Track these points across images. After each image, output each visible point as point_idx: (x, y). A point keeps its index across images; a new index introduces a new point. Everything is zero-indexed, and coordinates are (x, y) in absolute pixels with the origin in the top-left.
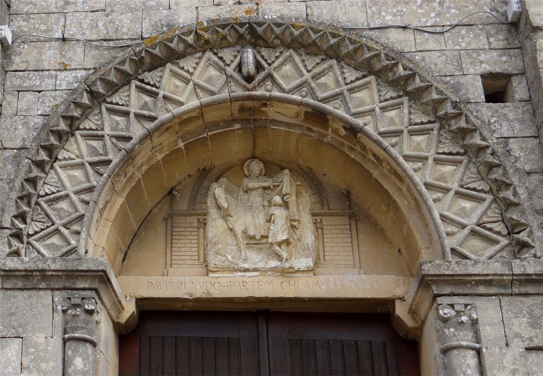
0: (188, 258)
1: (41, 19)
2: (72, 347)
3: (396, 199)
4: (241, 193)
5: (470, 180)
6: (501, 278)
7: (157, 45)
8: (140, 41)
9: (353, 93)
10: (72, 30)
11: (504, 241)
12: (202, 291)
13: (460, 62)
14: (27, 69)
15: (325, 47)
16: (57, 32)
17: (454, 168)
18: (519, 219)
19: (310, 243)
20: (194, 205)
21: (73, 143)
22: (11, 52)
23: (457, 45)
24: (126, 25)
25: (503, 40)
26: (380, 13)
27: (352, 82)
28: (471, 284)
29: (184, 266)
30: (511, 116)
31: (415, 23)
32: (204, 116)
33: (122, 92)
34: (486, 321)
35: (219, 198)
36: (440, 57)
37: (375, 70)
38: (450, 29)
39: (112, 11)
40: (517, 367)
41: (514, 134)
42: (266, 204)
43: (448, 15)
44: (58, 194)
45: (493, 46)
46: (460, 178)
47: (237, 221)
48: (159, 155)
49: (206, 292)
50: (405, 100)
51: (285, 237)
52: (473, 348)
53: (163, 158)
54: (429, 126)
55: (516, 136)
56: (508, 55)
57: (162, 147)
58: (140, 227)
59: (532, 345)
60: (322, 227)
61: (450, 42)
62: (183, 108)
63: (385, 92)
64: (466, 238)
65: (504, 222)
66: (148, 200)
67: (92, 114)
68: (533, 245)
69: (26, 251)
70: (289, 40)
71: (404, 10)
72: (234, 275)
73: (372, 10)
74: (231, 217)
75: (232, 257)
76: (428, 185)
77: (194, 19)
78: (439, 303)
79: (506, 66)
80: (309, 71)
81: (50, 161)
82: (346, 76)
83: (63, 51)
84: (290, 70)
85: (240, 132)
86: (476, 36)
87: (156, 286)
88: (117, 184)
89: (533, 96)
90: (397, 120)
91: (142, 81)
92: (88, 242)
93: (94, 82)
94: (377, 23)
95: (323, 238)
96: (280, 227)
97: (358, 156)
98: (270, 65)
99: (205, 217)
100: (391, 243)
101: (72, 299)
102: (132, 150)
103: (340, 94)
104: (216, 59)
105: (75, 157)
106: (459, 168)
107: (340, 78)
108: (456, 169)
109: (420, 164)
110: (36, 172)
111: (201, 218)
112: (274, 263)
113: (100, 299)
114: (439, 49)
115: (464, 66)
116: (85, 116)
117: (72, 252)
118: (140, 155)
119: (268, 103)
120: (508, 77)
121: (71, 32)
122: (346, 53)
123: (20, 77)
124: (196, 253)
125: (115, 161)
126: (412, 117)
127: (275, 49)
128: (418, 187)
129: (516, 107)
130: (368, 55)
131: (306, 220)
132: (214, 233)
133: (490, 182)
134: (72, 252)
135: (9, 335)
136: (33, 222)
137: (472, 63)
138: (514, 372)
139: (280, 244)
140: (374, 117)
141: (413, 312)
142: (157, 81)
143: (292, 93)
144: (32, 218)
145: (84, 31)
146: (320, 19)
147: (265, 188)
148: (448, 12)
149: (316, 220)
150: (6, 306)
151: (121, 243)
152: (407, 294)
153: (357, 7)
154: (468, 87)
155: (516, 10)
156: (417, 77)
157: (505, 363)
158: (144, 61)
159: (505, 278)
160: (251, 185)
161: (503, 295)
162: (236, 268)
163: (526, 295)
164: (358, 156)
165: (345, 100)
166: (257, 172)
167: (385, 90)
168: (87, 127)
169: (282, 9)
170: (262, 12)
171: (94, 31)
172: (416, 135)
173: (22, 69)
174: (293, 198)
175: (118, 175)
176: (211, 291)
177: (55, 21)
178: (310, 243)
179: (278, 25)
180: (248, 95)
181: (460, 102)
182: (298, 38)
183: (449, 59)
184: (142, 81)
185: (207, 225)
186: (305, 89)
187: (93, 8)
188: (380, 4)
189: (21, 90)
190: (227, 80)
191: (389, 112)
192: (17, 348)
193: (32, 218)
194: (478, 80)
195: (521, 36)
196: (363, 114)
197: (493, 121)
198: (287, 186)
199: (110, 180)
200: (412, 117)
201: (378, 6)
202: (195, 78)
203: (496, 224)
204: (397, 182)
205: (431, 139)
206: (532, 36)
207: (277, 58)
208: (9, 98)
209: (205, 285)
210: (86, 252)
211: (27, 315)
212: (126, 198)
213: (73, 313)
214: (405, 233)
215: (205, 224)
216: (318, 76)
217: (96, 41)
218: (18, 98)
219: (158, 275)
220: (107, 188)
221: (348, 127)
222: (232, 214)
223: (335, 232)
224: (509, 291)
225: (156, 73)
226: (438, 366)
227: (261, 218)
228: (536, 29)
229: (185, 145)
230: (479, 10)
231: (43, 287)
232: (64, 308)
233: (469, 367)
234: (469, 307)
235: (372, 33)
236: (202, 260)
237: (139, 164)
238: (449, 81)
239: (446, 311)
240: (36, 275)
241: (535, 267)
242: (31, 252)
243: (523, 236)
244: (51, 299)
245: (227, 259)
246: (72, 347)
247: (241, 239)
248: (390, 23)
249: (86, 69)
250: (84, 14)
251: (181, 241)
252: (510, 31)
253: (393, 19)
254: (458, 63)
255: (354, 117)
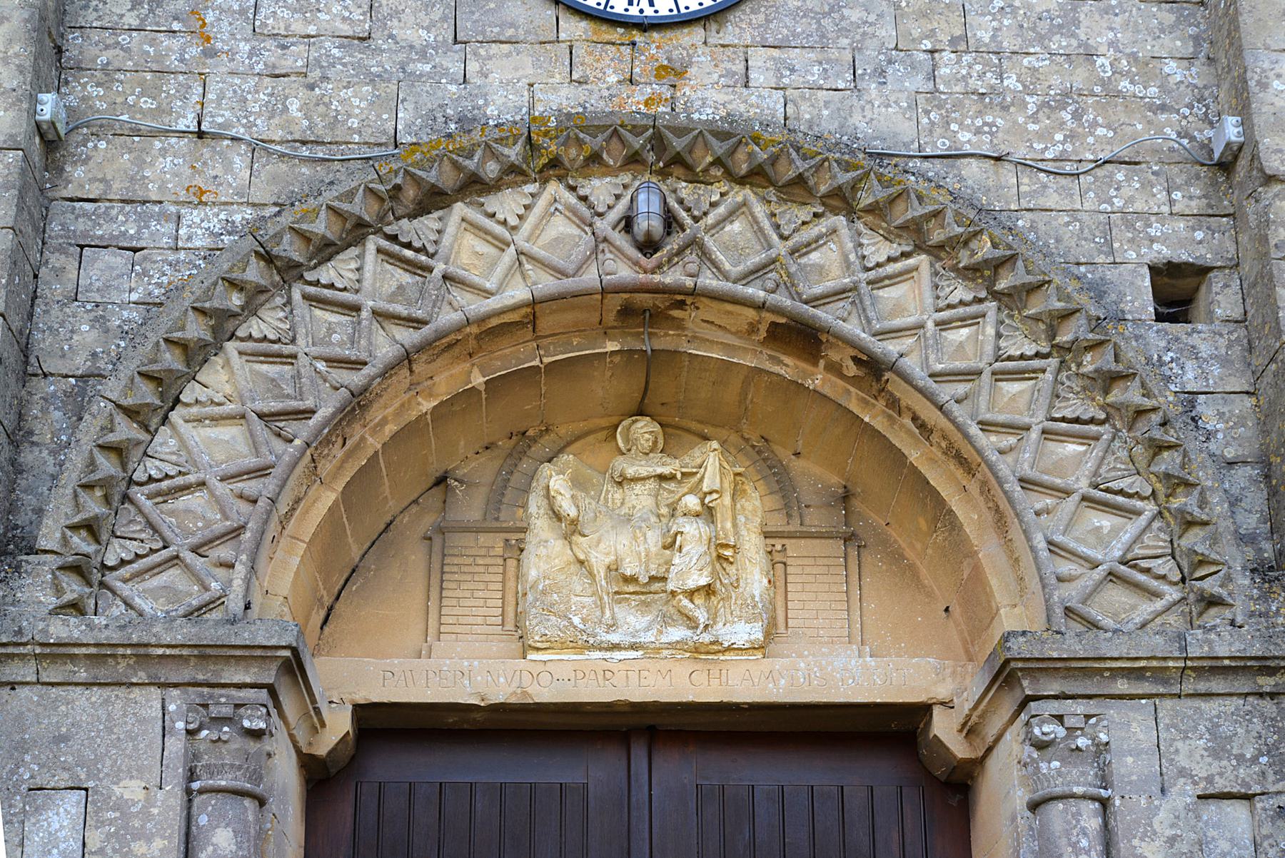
0: (480, 620)
1: (142, 83)
2: (210, 808)
3: (954, 509)
4: (608, 486)
5: (1113, 474)
6: (1163, 664)
7: (435, 161)
8: (391, 150)
9: (879, 288)
10: (223, 115)
11: (1172, 594)
12: (510, 690)
13: (1108, 237)
14: (104, 197)
15: (823, 189)
16: (185, 117)
17: (1082, 448)
18: (1207, 553)
19: (757, 593)
20: (499, 510)
21: (219, 368)
22: (64, 156)
23: (1104, 203)
24: (357, 111)
25: (1200, 198)
26: (948, 123)
27: (878, 265)
28: (1102, 676)
29: (470, 637)
30: (1205, 349)
31: (1020, 152)
32: (537, 322)
33: (343, 261)
34: (1125, 747)
35: (559, 498)
36: (1068, 224)
37: (930, 243)
38: (1092, 169)
39: (325, 78)
40: (1179, 832)
41: (1207, 386)
42: (664, 511)
43: (1091, 140)
44: (180, 481)
45: (1176, 209)
46: (1093, 469)
47: (597, 546)
48: (424, 402)
49: (519, 691)
50: (990, 308)
51: (703, 581)
52: (1093, 798)
53: (435, 407)
54: (1037, 363)
55: (1212, 390)
56: (1208, 228)
57: (434, 384)
58: (366, 553)
59: (1211, 791)
60: (784, 560)
61: (1092, 194)
62: (493, 303)
63: (948, 290)
64: (1097, 587)
65: (1174, 558)
66: (389, 497)
67: (268, 305)
68: (1232, 602)
69: (96, 604)
70: (744, 168)
71: (999, 121)
72: (586, 657)
73: (929, 119)
74: (584, 536)
75: (582, 619)
76: (1025, 482)
77: (524, 110)
78: (1034, 713)
79: (1202, 250)
80: (783, 238)
81: (161, 407)
82: (866, 253)
83: (197, 161)
84: (740, 233)
85: (617, 359)
86: (1146, 185)
87: (403, 678)
88: (323, 461)
89: (1251, 312)
90: (969, 349)
91: (393, 238)
92: (252, 586)
93: (278, 236)
94: (942, 146)
95: (786, 583)
96: (694, 561)
97: (879, 418)
98: (696, 219)
99: (521, 536)
100: (930, 595)
101: (211, 708)
102: (365, 389)
103: (850, 290)
104: (572, 200)
105: (223, 400)
106: (1093, 449)
107: (852, 257)
108: (1086, 452)
109: (1012, 440)
110: (126, 430)
111: (513, 537)
112: (677, 633)
113: (278, 705)
114: (1068, 208)
115: (1116, 245)
116: (250, 309)
117: (212, 606)
118: (382, 401)
119: (689, 300)
120: (1202, 271)
121: (220, 120)
122: (870, 205)
123: (85, 214)
124: (499, 595)
125: (324, 413)
126: (1002, 343)
127: (709, 187)
128: (1007, 486)
129: (1215, 333)
130: (919, 211)
131: (752, 544)
132: (541, 570)
133: (1154, 479)
134: (212, 606)
135: (52, 784)
136: (115, 540)
137: (1131, 241)
138: (1172, 841)
139: (691, 594)
140: (922, 340)
141: (970, 730)
142: (430, 241)
143: (744, 282)
144: (113, 531)
145: (252, 119)
146: (816, 129)
147: (662, 478)
148: (1091, 134)
149: (773, 546)
150: (46, 721)
151: (322, 587)
152: (959, 695)
153: (898, 109)
154: (1122, 288)
155: (1233, 139)
156: (1020, 264)
157: (1156, 826)
158: (400, 196)
159: (1171, 664)
160: (630, 472)
161: (1162, 696)
162: (591, 642)
163: (1209, 695)
164: (879, 418)
165: (861, 302)
166: (646, 445)
167: (949, 286)
168: (256, 334)
169: (730, 102)
170: (686, 103)
171: (276, 121)
172: (1007, 380)
173: (91, 197)
174: (727, 500)
175: (327, 442)
176: (529, 690)
177: (177, 91)
178: (757, 593)
179: (722, 136)
180: (644, 280)
181: (1105, 319)
182: (766, 167)
183: (1087, 230)
184: (393, 238)
185: (525, 552)
186: (773, 275)
187: (274, 67)
188: (948, 106)
189: (87, 243)
190: (597, 246)
191: (954, 331)
192: (73, 811)
193: (113, 531)
194: (1143, 277)
195: (1236, 192)
196: (899, 334)
197: (1167, 359)
198: (714, 475)
199: (308, 453)
200: (1002, 343)
201: (943, 111)
202: (520, 238)
203: (1160, 561)
204: (959, 473)
205: (1039, 390)
206: (1260, 193)
207: (713, 205)
208: (56, 260)
209: (517, 678)
210: (247, 607)
211: (99, 740)
212: (342, 493)
213: (215, 737)
214: (965, 577)
215: (522, 550)
216: (805, 250)
217: (281, 143)
218: (80, 263)
219: (405, 657)
220: (299, 469)
221: (865, 358)
222: (586, 532)
223: (815, 570)
224: (1176, 690)
225: (429, 223)
226: (1018, 834)
227: (653, 539)
228: (1270, 179)
229: (486, 383)
230: (1155, 134)
231: (140, 681)
232: (191, 727)
233: (1085, 834)
234: (1093, 721)
235: (926, 165)
236: (510, 626)
237: (377, 420)
238: (1085, 275)
239: (1046, 729)
240: (124, 656)
241: (1230, 644)
242: (110, 606)
243: (1211, 586)
244: (159, 706)
245: (572, 623)
246: (210, 808)
247: (603, 583)
248: (969, 147)
249: (254, 205)
250: (252, 81)
251: (464, 586)
252: (1214, 184)
253: (974, 139)
254: (1106, 239)
255: (878, 338)
